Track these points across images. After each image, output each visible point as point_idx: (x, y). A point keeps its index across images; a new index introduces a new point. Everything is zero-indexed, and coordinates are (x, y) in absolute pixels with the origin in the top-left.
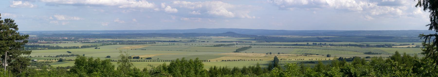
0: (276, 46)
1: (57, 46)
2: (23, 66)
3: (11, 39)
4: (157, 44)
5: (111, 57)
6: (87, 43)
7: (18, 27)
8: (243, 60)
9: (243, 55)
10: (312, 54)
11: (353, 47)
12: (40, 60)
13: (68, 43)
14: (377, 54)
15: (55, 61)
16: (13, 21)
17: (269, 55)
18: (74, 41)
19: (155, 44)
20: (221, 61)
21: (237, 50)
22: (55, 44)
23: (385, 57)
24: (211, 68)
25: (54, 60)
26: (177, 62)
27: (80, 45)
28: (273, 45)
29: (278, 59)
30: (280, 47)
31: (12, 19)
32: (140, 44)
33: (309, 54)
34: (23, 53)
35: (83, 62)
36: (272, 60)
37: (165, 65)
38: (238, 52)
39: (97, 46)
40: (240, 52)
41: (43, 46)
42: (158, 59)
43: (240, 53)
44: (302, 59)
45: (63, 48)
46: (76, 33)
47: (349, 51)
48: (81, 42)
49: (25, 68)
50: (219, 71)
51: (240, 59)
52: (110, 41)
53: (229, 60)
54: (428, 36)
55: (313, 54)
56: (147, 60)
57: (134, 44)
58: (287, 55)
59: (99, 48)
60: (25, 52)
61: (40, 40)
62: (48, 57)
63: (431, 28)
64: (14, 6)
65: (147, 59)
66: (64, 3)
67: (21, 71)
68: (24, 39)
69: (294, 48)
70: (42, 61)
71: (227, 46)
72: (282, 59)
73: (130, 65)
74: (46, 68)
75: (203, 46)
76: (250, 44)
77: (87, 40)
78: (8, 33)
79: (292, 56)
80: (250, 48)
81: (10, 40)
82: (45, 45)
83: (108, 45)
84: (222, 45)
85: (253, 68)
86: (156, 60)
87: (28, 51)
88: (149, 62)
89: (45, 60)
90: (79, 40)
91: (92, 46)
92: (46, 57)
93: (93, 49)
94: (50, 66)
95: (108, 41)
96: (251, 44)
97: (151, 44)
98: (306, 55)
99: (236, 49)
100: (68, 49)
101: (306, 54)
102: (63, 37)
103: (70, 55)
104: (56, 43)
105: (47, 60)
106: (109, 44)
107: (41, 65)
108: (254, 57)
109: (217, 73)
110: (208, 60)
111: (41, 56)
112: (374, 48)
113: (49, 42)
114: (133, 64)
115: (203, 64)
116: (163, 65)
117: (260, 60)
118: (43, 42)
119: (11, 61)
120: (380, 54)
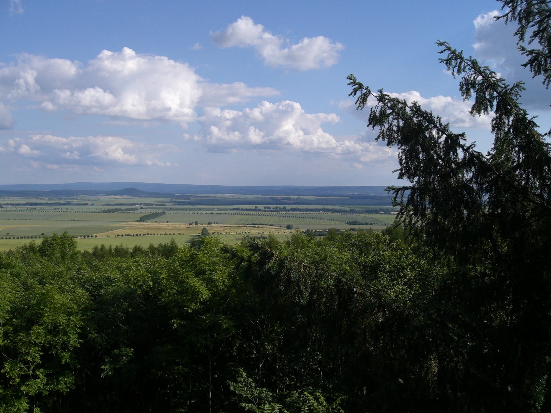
0: (205, 212)
4: (5, 209)
8: (151, 234)
11: (329, 213)
14: (367, 224)
17: (193, 226)
21: (141, 218)
24: (96, 249)
26: (54, 239)
28: (200, 209)
30: (211, 213)
36: (199, 234)
37: (34, 244)
40: (147, 222)
51: (146, 233)
54: (400, 189)
71: (125, 212)
72: (215, 233)
75: (84, 212)
76: (163, 209)
80: (163, 215)
84: (116, 210)
86: (5, 237)
96: (165, 208)
110: (94, 235)
116: (29, 244)
117: (179, 234)
120: (372, 224)
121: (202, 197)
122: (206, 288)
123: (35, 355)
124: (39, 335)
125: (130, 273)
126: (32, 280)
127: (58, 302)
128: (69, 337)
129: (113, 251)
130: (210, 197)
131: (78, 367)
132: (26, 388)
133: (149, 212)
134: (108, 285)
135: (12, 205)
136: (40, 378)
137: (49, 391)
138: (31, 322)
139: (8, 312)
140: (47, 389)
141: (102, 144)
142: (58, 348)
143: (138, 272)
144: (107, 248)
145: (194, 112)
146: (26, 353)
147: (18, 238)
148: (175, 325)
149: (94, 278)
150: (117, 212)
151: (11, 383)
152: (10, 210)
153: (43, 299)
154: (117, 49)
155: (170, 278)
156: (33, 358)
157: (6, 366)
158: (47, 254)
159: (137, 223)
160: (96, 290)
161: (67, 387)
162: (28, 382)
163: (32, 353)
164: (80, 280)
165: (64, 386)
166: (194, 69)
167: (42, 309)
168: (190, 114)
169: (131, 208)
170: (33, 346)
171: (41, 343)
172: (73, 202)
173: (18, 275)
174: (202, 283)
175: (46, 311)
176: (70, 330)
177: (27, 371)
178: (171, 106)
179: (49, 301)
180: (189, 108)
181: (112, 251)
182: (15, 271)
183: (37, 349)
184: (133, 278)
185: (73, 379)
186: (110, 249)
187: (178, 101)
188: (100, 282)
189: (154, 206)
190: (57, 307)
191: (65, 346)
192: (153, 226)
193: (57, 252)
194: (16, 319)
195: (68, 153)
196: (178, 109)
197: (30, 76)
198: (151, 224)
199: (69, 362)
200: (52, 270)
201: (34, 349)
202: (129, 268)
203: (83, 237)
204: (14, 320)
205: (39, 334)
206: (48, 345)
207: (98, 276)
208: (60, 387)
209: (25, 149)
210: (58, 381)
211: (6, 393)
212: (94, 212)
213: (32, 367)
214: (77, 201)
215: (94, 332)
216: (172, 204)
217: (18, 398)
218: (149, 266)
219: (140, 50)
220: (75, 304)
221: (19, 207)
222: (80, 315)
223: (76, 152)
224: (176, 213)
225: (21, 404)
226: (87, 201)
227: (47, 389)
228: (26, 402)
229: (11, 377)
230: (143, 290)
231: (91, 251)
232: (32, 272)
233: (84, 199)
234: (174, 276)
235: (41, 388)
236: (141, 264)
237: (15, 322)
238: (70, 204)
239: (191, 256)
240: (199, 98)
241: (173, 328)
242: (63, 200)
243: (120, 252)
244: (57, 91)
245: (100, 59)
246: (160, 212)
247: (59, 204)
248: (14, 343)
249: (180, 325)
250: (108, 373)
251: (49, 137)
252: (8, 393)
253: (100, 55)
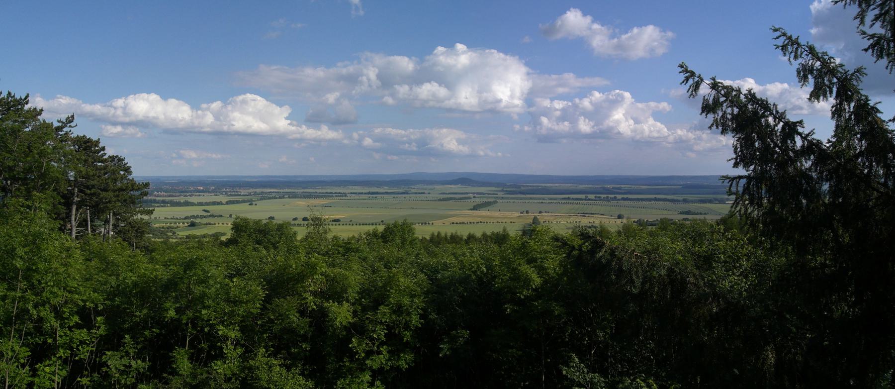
0: (536, 201)
2: (139, 234)
3: (124, 190)
4: (349, 198)
5: (275, 219)
6: (235, 195)
10: (593, 214)
11: (661, 202)
12: (157, 224)
13: (204, 196)
14: (701, 214)
16: (123, 160)
18: (213, 192)
19: (347, 198)
21: (474, 206)
22: (182, 197)
23: (712, 218)
24: (433, 235)
25: (181, 224)
27: (223, 199)
33: (589, 214)
34: (139, 212)
35: (245, 227)
37: (377, 231)
38: (477, 210)
41: (163, 200)
44: (577, 221)
46: (217, 180)
47: (655, 209)
48: (226, 194)
49: (141, 237)
52: (273, 192)
53: (463, 223)
54: (735, 178)
55: (596, 214)
56: (334, 223)
57: (312, 198)
58: (553, 214)
59: (256, 205)
61: (158, 192)
62: (172, 219)
63: (736, 165)
65: (333, 221)
66: (196, 130)
68: (142, 190)
69: (564, 203)
70: (162, 225)
72: (546, 221)
74: (168, 237)
76: (495, 198)
77: (237, 192)
79: (562, 217)
82: (165, 200)
83: (270, 198)
84: (451, 199)
91: (244, 201)
92: (168, 219)
93: (245, 206)
94: (174, 233)
95: (270, 192)
96: (497, 197)
97: (339, 198)
98: (584, 215)
101: (584, 214)
102: (197, 186)
103: (207, 216)
107: (162, 232)
110: (431, 223)
111: (159, 218)
112: (695, 204)
114: (331, 229)
115: (414, 229)
117: (511, 222)
118: (162, 194)
119: (118, 226)
120: (706, 214)
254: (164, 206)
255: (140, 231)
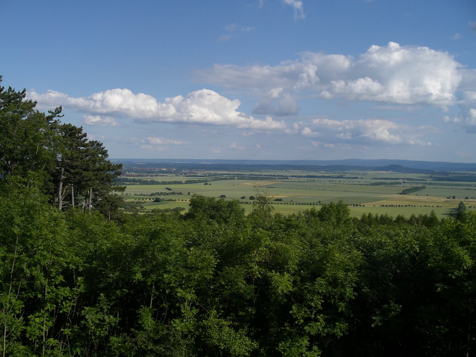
0: (463, 187)
1: (151, 180)
3: (102, 170)
4: (290, 180)
5: (226, 197)
6: (193, 176)
7: (107, 152)
8: (412, 206)
9: (413, 198)
13: (167, 176)
15: (149, 201)
16: (101, 145)
17: (451, 200)
18: (175, 173)
19: (288, 180)
20: (381, 206)
21: (403, 191)
22: (149, 177)
24: (364, 216)
25: (148, 199)
26: (331, 206)
27: (183, 179)
28: (458, 185)
29: (464, 206)
30: (468, 189)
31: (99, 142)
32: (267, 179)
35: (201, 204)
36: (456, 207)
37: (315, 210)
38: (406, 194)
39: (208, 181)
40: (408, 195)
41: (133, 179)
42: (291, 201)
43: (408, 196)
45: (160, 183)
48: (184, 175)
49: (115, 210)
50: (375, 220)
51: (408, 205)
52: (225, 174)
59: (210, 184)
60: (118, 188)
61: (129, 172)
62: (140, 195)
64: (91, 122)
65: (276, 200)
67: (109, 215)
70: (132, 200)
71: (390, 185)
72: (471, 207)
73: (270, 208)
75: (355, 184)
76: (423, 183)
77: (194, 173)
78: (97, 161)
80: (423, 189)
81: (99, 171)
82: (135, 179)
83: (222, 179)
84: (382, 183)
85: (425, 217)
86: (289, 203)
87: (122, 187)
88: (279, 205)
89: (135, 199)
90: (183, 173)
91: (200, 181)
94: (142, 207)
95: (222, 174)
96: (426, 183)
97: (281, 180)
99: (403, 190)
100: (167, 184)
102: (161, 168)
103: (169, 193)
104: (151, 176)
105: (139, 199)
106: (224, 178)
107: (132, 206)
108: (429, 202)
109: (372, 222)
110: (362, 205)
111: (130, 194)
113: (141, 175)
115: (349, 210)
116: (311, 209)
117: (438, 206)
118: (132, 174)
119: (97, 200)
121: (461, 174)
122: (470, 257)
123: (317, 302)
124: (321, 286)
125: (399, 239)
126: (316, 240)
127: (338, 260)
128: (345, 290)
129: (379, 219)
130: (468, 174)
131: (351, 316)
132: (308, 328)
133: (411, 186)
134: (379, 248)
135: (294, 176)
136: (320, 322)
137: (327, 333)
138: (314, 275)
139: (297, 265)
140: (325, 331)
141: (370, 126)
142: (336, 298)
143: (406, 239)
144: (374, 216)
145: (454, 96)
146: (311, 299)
147: (299, 204)
148: (439, 289)
149: (368, 242)
150: (382, 185)
151: (296, 323)
152: (294, 181)
153: (326, 256)
154: (384, 43)
155: (437, 245)
156: (316, 305)
157: (293, 309)
158: (325, 219)
159: (400, 195)
160: (368, 252)
161: (341, 332)
162: (310, 323)
163: (315, 300)
164: (355, 242)
165: (339, 330)
166: (453, 57)
167: (325, 264)
168: (450, 99)
169: (381, 182)
170: (316, 294)
171: (322, 292)
172: (345, 175)
173: (303, 235)
174: (466, 252)
175: (328, 266)
176: (347, 284)
177: (310, 315)
178: (432, 92)
179: (330, 258)
180: (450, 92)
181: (378, 219)
182: (302, 231)
183: (320, 298)
184: (402, 244)
185: (347, 326)
186: (377, 217)
187: (439, 87)
188: (372, 245)
189: (416, 181)
190: (337, 263)
191: (342, 298)
192: (414, 198)
193: (333, 218)
194: (304, 271)
195: (342, 134)
196: (439, 94)
197: (311, 70)
198: (412, 197)
199: (344, 310)
200: (332, 232)
201: (317, 297)
202: (397, 235)
203: (352, 206)
204: (302, 272)
205: (321, 285)
206: (328, 295)
207: (371, 240)
208: (336, 331)
209: (307, 131)
210: (335, 326)
211: (292, 330)
212: (363, 185)
213: (314, 312)
214: (349, 174)
215: (366, 287)
216: (432, 179)
217: (301, 335)
218: (415, 234)
219: (403, 43)
220: (352, 262)
221: (301, 179)
222: (356, 272)
223: (348, 133)
224: (435, 188)
225: (303, 341)
226: (357, 175)
227: (325, 331)
228: (307, 340)
229: (297, 317)
230: (410, 255)
231: (359, 218)
232: (315, 233)
233: (354, 173)
234: (441, 245)
235: (320, 330)
236: (409, 232)
237: (302, 273)
238: (342, 178)
239: (457, 227)
240: (459, 83)
241: (437, 291)
242: (337, 174)
243: (384, 220)
244: (333, 82)
245: (370, 53)
246: (421, 187)
247: (334, 177)
248: (301, 290)
249: (444, 289)
250: (377, 324)
251: (326, 120)
252: (294, 330)
253: (370, 50)
254: (134, 184)
255: (114, 205)
